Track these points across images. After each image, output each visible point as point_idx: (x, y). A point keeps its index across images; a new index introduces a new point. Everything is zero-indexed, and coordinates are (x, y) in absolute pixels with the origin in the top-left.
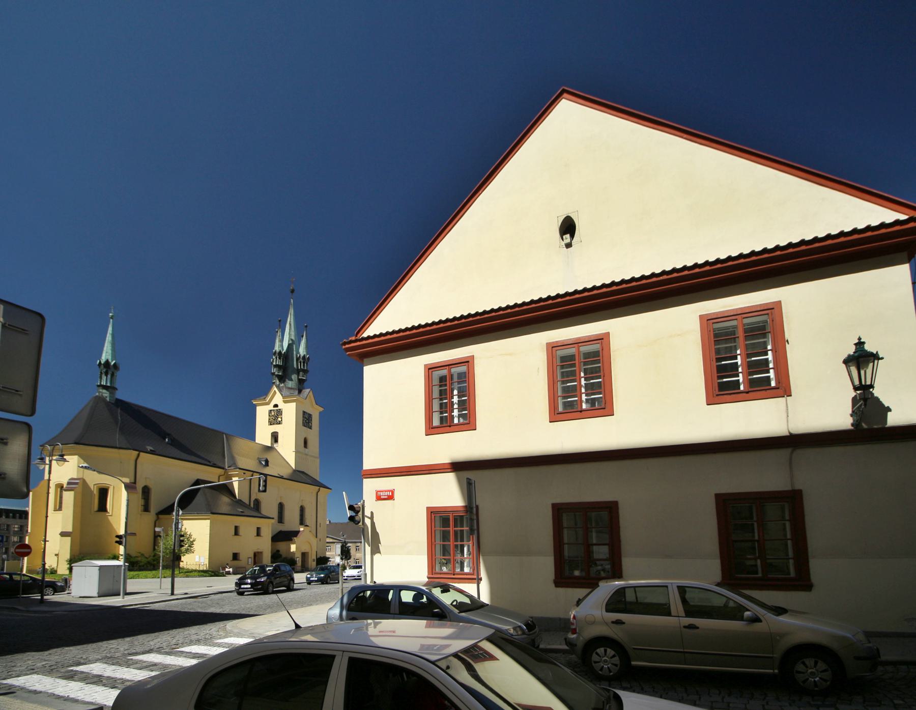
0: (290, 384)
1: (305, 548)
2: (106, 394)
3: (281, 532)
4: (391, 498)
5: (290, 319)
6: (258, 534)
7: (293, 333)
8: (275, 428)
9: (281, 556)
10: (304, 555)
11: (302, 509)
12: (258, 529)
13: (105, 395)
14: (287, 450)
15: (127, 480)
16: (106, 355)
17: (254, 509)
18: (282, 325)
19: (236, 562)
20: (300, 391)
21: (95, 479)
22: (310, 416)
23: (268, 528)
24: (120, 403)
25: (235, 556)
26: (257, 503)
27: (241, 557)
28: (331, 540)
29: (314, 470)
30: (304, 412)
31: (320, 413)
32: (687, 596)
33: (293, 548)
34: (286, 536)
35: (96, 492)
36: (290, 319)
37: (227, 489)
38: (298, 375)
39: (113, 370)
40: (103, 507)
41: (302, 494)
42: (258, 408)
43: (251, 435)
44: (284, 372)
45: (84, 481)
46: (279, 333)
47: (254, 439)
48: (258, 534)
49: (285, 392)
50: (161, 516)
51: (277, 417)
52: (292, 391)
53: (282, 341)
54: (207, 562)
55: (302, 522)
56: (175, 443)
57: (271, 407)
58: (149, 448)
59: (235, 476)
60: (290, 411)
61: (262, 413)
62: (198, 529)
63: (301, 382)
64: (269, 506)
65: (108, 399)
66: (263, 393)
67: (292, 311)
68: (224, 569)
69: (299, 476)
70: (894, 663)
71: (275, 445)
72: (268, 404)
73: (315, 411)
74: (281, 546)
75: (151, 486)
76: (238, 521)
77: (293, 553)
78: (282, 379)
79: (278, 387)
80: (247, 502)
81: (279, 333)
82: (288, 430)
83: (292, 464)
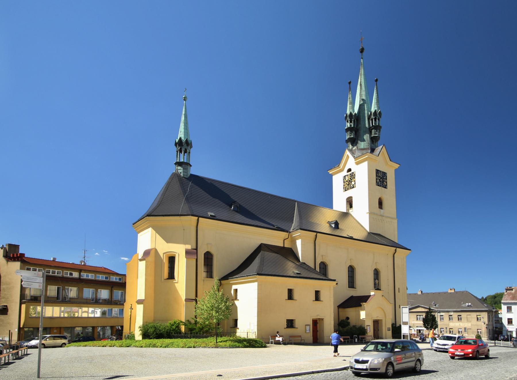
0: (362, 145)
1: (377, 316)
2: (180, 170)
3: (352, 297)
5: (361, 79)
6: (317, 296)
7: (364, 93)
8: (350, 193)
9: (348, 324)
10: (377, 323)
11: (377, 274)
12: (317, 293)
13: (179, 171)
14: (362, 215)
15: (189, 247)
16: (181, 135)
17: (322, 272)
18: (351, 86)
19: (291, 331)
20: (373, 150)
21: (164, 248)
22: (384, 174)
23: (331, 292)
24: (196, 180)
25: (290, 324)
26: (324, 266)
27: (297, 324)
29: (393, 234)
30: (377, 171)
31: (396, 170)
32: (181, 314)
33: (363, 315)
34: (357, 302)
35: (166, 261)
36: (361, 79)
37: (289, 253)
38: (371, 133)
39: (185, 146)
40: (171, 276)
41: (380, 256)
42: (334, 177)
43: (330, 205)
44: (356, 134)
45: (156, 250)
46: (350, 96)
48: (317, 296)
49: (358, 153)
51: (350, 181)
52: (364, 152)
53: (353, 103)
55: (377, 287)
56: (242, 210)
57: (345, 173)
58: (210, 214)
59: (299, 237)
60: (362, 172)
61: (338, 180)
62: (247, 295)
63: (374, 140)
64: (338, 271)
65: (182, 175)
66: (336, 161)
67: (362, 71)
68: (274, 337)
69: (374, 238)
71: (350, 211)
72: (342, 170)
73: (390, 169)
74: (350, 312)
75: (213, 251)
76: (291, 283)
77: (363, 321)
78: (354, 141)
79: (351, 151)
80: (312, 266)
81: (350, 96)
82: (362, 193)
83: (368, 229)
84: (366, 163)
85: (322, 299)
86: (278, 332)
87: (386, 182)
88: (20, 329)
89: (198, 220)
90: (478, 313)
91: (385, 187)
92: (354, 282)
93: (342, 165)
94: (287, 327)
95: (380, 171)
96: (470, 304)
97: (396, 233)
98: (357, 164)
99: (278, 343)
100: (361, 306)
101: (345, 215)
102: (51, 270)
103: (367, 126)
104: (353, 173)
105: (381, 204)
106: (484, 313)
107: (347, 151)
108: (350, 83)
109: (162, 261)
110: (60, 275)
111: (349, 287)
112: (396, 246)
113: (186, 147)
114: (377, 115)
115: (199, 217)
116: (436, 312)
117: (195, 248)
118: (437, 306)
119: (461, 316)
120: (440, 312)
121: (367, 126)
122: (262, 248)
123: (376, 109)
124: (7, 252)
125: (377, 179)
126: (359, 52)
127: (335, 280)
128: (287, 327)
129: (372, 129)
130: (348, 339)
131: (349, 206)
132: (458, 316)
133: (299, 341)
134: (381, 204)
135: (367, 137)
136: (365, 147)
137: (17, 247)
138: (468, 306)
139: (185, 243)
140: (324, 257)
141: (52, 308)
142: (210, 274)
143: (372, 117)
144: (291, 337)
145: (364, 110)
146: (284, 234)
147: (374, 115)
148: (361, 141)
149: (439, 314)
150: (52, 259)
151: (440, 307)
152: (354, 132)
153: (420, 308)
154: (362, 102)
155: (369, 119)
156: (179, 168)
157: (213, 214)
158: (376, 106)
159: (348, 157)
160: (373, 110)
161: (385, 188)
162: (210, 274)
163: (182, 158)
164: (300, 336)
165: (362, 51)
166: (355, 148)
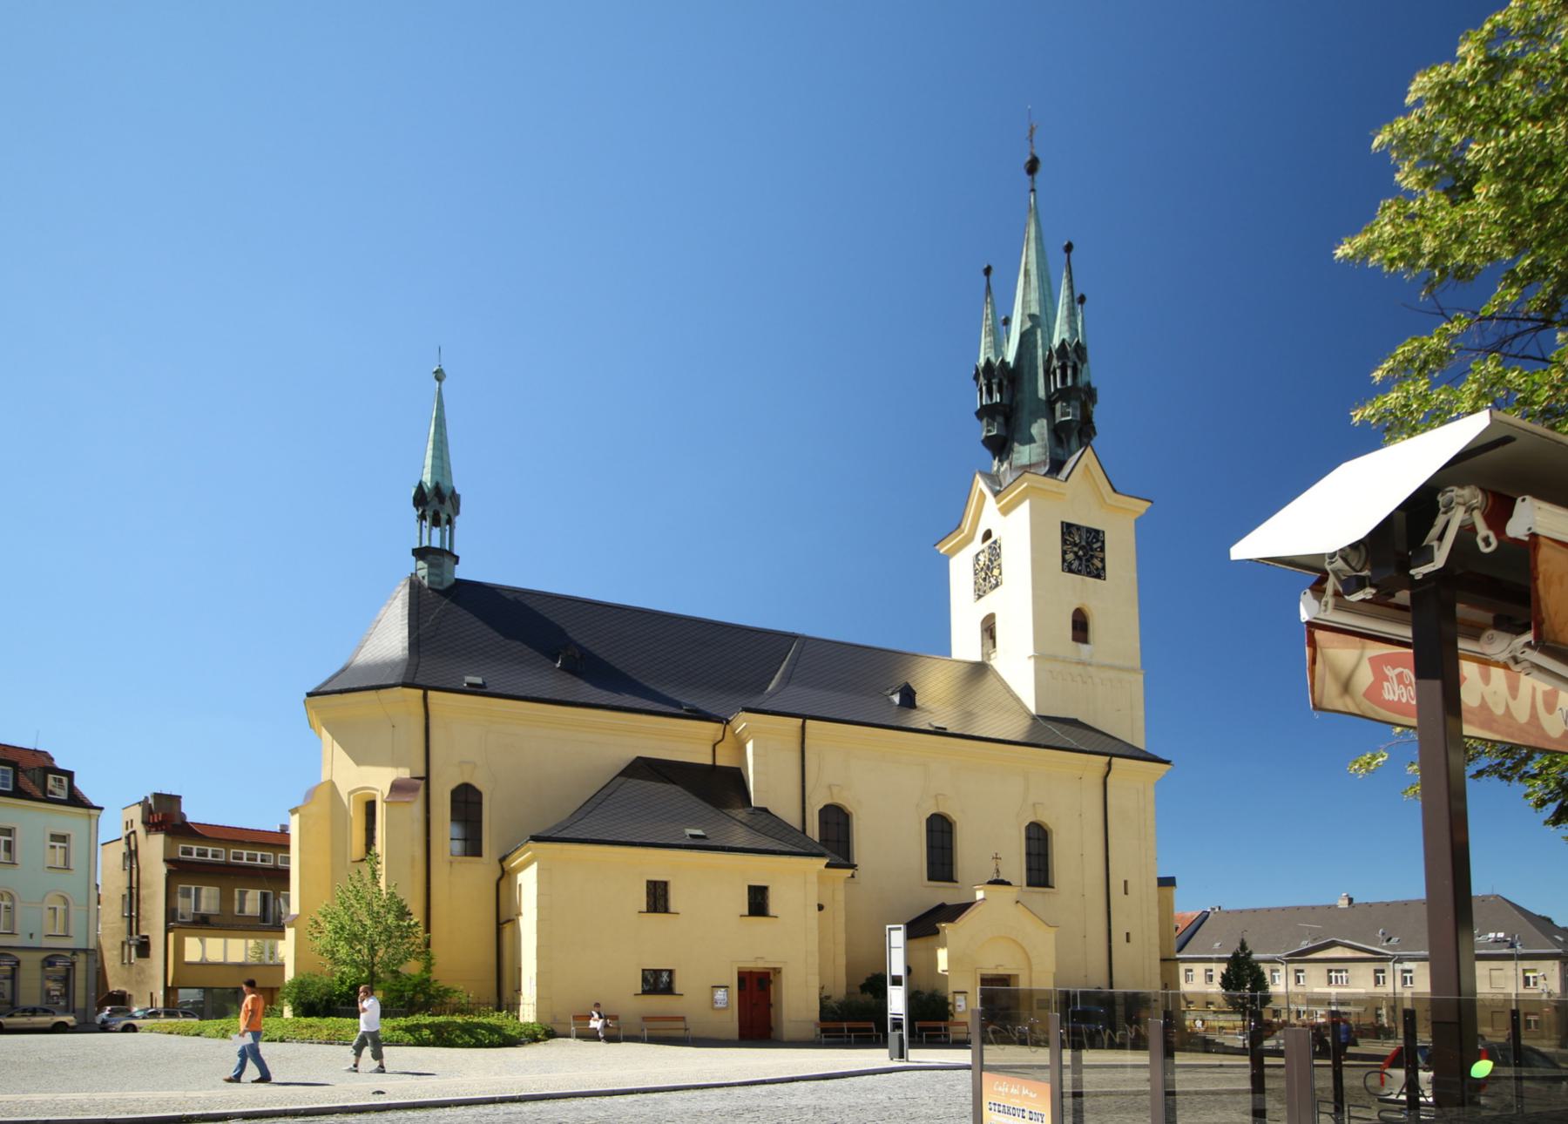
0: (1024, 454)
4: (310, 695)
5: (1029, 257)
6: (758, 902)
7: (1034, 296)
8: (991, 603)
11: (1038, 840)
14: (1017, 668)
15: (404, 773)
20: (1056, 467)
22: (1096, 536)
26: (837, 822)
28: (1349, 954)
29: (1121, 709)
30: (1068, 529)
31: (1140, 523)
37: (720, 787)
39: (435, 503)
41: (1062, 788)
43: (946, 649)
47: (949, 654)
48: (758, 902)
51: (989, 568)
54: (844, 991)
61: (961, 570)
65: (426, 582)
66: (950, 519)
69: (1056, 732)
70: (1096, 1095)
72: (969, 540)
76: (760, 869)
78: (1000, 447)
80: (793, 818)
84: (1024, 508)
86: (597, 1005)
87: (1103, 560)
88: (167, 989)
89: (425, 697)
90: (1527, 964)
91: (1099, 574)
92: (1046, 871)
93: (966, 525)
94: (644, 992)
95: (1079, 528)
96: (1501, 935)
97: (1140, 713)
99: (592, 1036)
100: (937, 932)
101: (979, 670)
102: (195, 848)
103: (1042, 393)
105: (1080, 627)
106: (1550, 963)
107: (978, 477)
108: (988, 271)
109: (346, 812)
110: (222, 859)
111: (930, 879)
112: (1113, 749)
113: (438, 507)
114: (1072, 356)
115: (805, 717)
116: (1388, 960)
117: (422, 774)
118: (1394, 940)
119: (1410, 971)
120: (1400, 960)
121: (1042, 393)
122: (644, 769)
123: (1066, 336)
124: (151, 812)
125: (1064, 553)
126: (1024, 172)
128: (644, 992)
129: (1055, 402)
130: (870, 1030)
132: (1376, 971)
133: (681, 1033)
134: (1080, 627)
135: (1040, 428)
136: (1034, 459)
137: (176, 799)
138: (1496, 941)
139: (396, 764)
140: (835, 790)
141: (221, 941)
143: (1055, 363)
144: (645, 1019)
145: (1035, 347)
146: (710, 729)
147: (1059, 358)
148: (1022, 444)
149: (1399, 967)
150: (278, 829)
151: (1403, 945)
152: (1000, 419)
153: (1339, 948)
154: (1028, 325)
155: (1047, 373)
156: (421, 564)
157: (479, 680)
158: (1066, 327)
159: (982, 495)
160: (1056, 342)
161: (1098, 576)
162: (473, 846)
163: (435, 539)
164: (683, 1019)
165: (1033, 166)
166: (1006, 465)
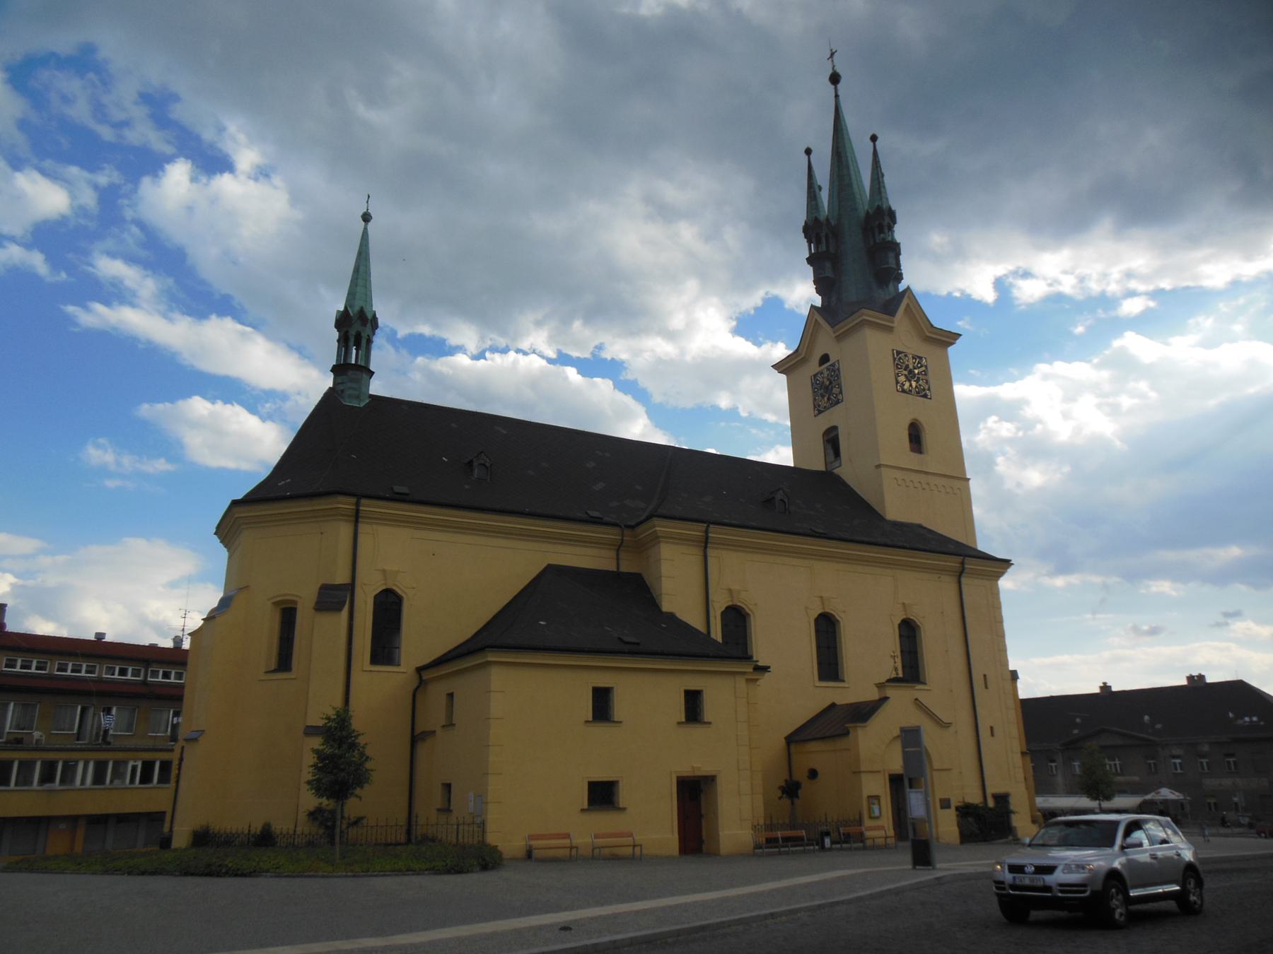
8: (834, 417)
19: (604, 821)
26: (736, 618)
50: (426, 676)
74: (817, 755)
85: (708, 715)
98: (839, 338)
104: (833, 365)
115: (709, 523)
127: (288, 615)
131: (831, 452)
142: (384, 651)
157: (404, 490)
